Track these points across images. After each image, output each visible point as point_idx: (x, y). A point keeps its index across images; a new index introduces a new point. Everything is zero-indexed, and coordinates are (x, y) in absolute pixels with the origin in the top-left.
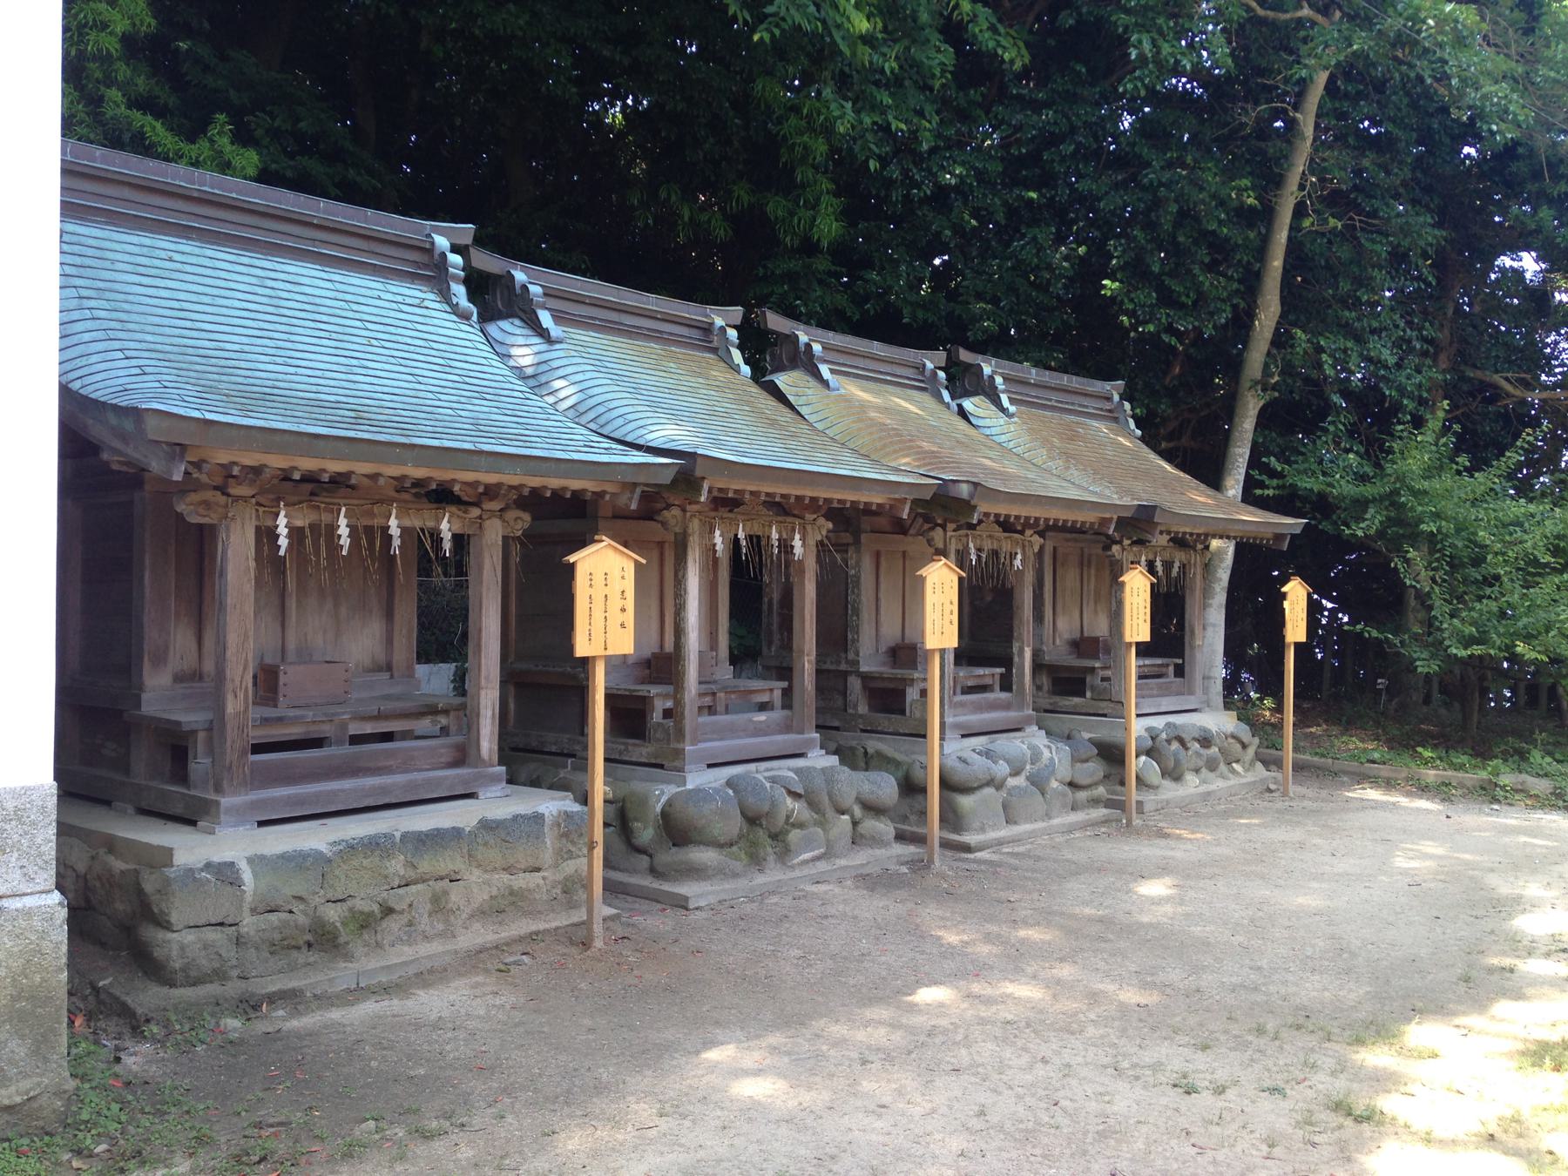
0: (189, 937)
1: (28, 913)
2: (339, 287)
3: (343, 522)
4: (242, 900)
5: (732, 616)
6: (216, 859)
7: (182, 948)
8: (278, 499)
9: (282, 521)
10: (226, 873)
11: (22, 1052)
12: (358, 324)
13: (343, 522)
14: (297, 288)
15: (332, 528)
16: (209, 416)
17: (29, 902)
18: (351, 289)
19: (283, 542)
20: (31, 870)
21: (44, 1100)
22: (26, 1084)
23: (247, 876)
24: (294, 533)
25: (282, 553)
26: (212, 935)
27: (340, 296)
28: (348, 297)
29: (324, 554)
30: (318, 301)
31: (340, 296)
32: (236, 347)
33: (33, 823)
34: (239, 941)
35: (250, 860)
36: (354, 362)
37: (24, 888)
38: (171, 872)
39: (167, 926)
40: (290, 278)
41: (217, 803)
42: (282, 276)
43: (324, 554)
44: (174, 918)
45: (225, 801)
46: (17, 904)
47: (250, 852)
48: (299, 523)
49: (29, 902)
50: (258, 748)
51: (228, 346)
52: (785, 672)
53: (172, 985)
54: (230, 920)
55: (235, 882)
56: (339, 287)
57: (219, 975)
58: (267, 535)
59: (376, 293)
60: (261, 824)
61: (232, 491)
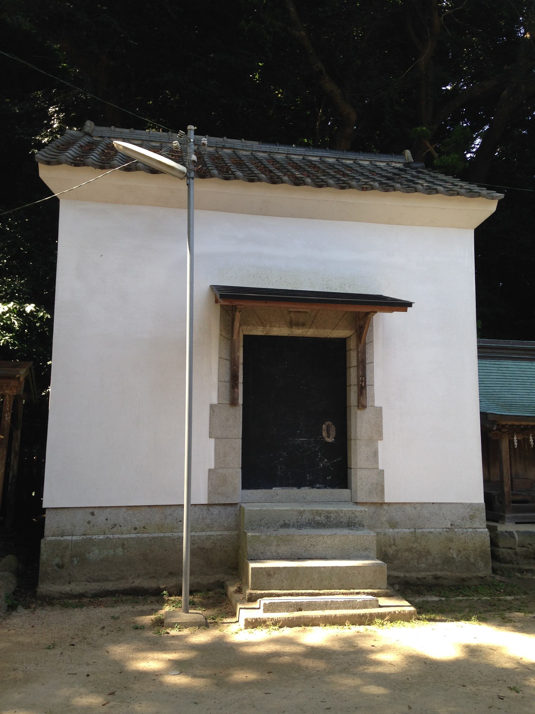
0: (504, 550)
1: (482, 532)
2: (520, 367)
3: (531, 438)
4: (516, 542)
5: (333, 568)
6: (508, 530)
7: (503, 553)
8: (514, 432)
9: (515, 438)
10: (511, 534)
11: (483, 565)
12: (527, 378)
13: (531, 438)
14: (508, 369)
15: (529, 439)
16: (503, 413)
17: (482, 530)
18: (523, 367)
19: (516, 444)
20: (481, 522)
21: (488, 577)
22: (484, 573)
23: (516, 536)
24: (519, 441)
25: (516, 447)
26: (509, 551)
27: (520, 370)
28: (522, 370)
29: (526, 447)
30: (515, 372)
31: (520, 370)
32: (498, 391)
33: (481, 512)
34: (516, 554)
35: (517, 532)
36: (529, 391)
37: (480, 527)
38: (498, 532)
39: (498, 547)
40: (506, 366)
41: (504, 516)
42: (503, 366)
43: (526, 447)
44: (500, 544)
45: (507, 516)
46: (479, 530)
47: (516, 530)
48: (519, 439)
49: (482, 530)
50: (514, 502)
51: (496, 391)
52: (367, 314)
53: (501, 563)
54: (513, 547)
55: (514, 537)
56: (520, 367)
57: (511, 562)
58: (511, 442)
59: (529, 367)
60: (517, 523)
61: (502, 430)
